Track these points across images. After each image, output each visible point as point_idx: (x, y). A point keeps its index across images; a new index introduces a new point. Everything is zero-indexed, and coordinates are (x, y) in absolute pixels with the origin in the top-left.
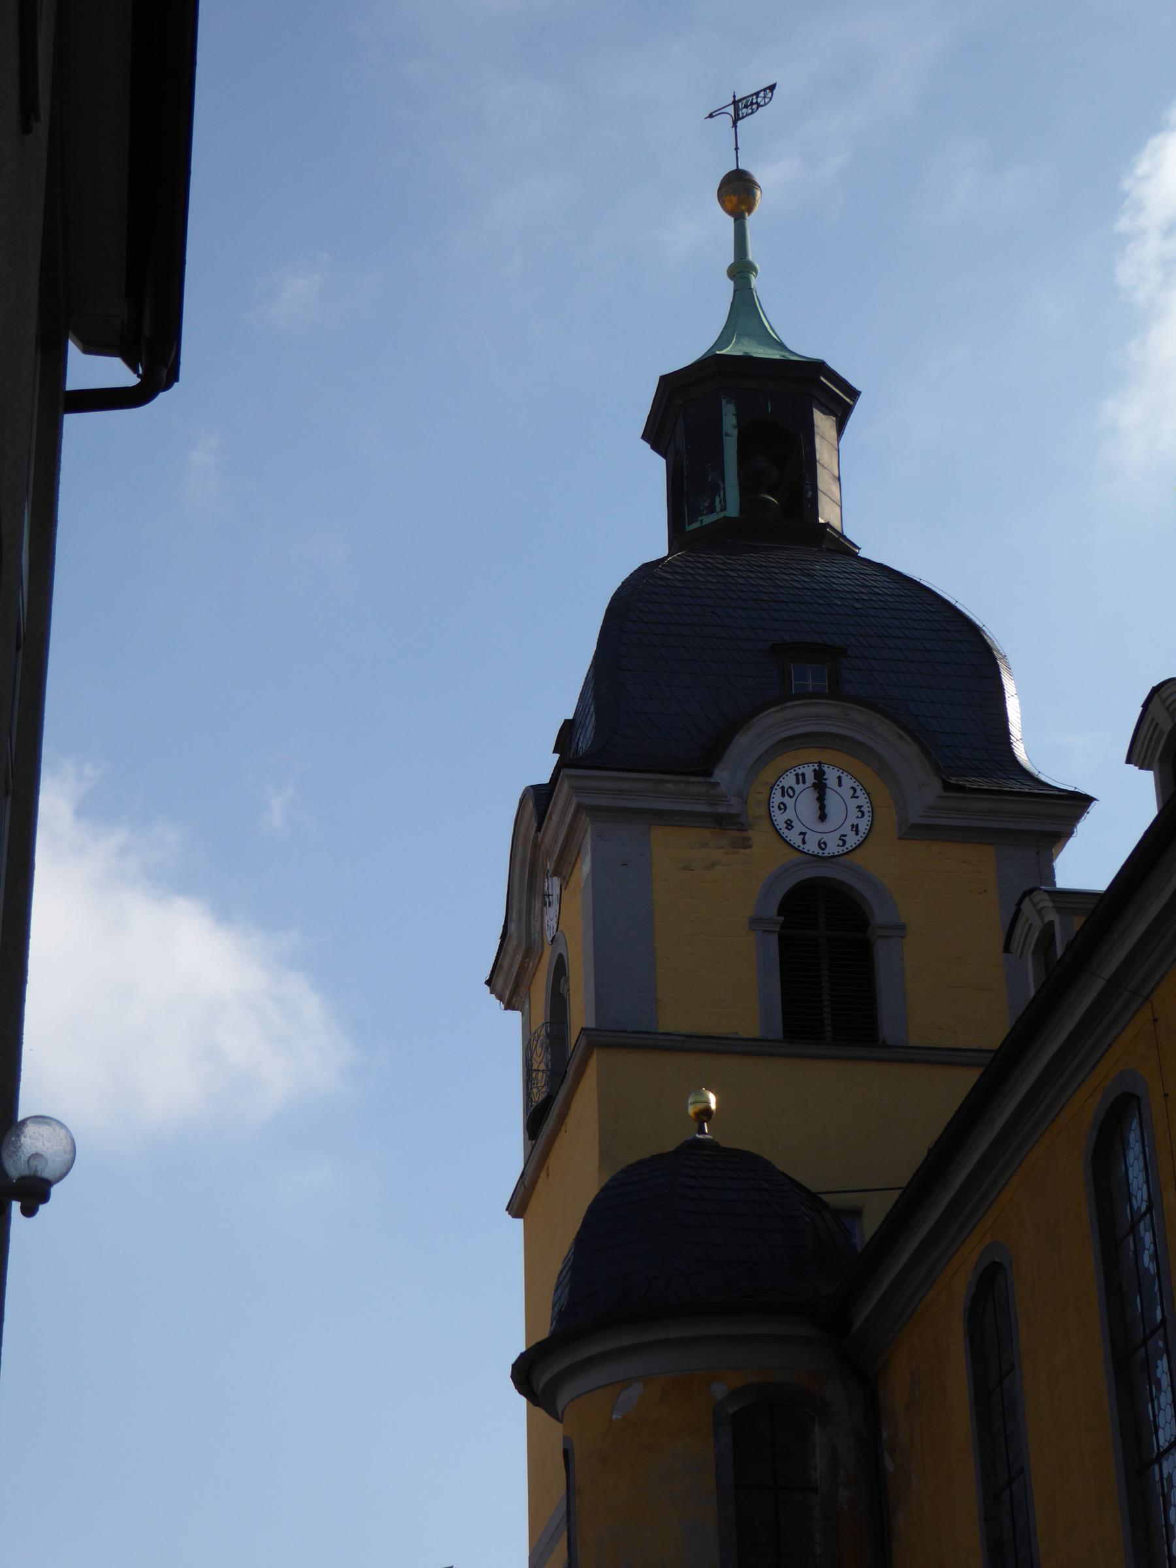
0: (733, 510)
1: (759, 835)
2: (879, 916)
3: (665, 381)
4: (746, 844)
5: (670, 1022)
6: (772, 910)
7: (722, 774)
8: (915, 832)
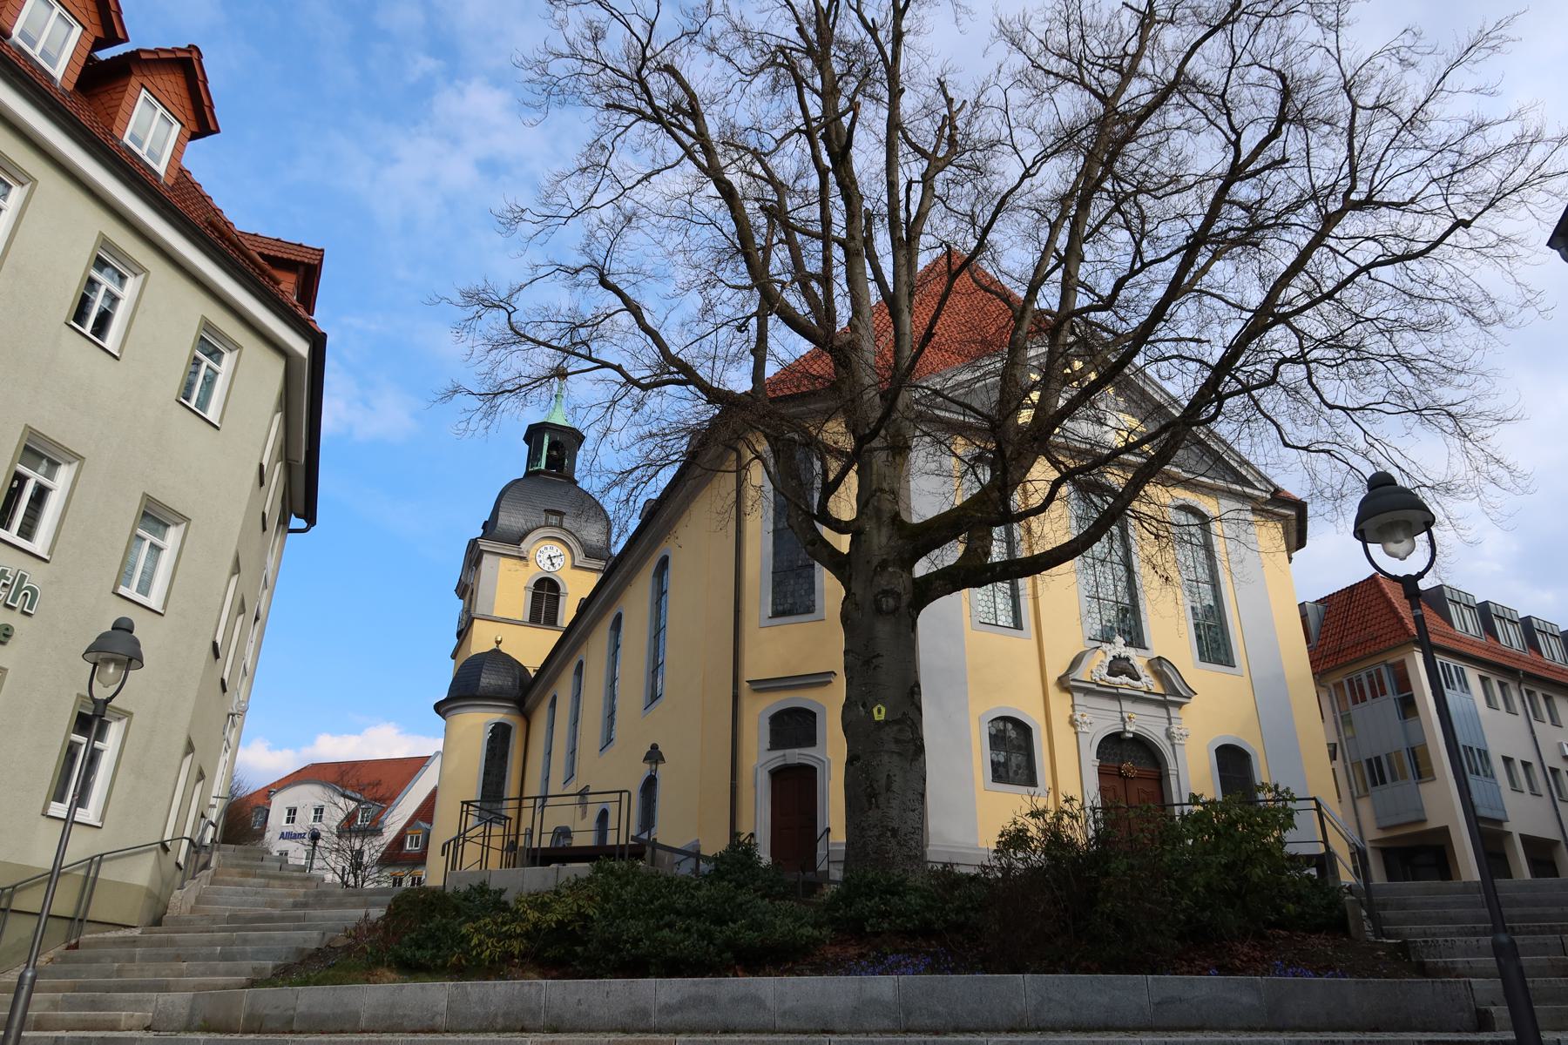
0: (543, 467)
1: (532, 564)
2: (562, 590)
3: (530, 426)
4: (527, 565)
5: (497, 614)
6: (532, 585)
7: (522, 545)
8: (575, 567)
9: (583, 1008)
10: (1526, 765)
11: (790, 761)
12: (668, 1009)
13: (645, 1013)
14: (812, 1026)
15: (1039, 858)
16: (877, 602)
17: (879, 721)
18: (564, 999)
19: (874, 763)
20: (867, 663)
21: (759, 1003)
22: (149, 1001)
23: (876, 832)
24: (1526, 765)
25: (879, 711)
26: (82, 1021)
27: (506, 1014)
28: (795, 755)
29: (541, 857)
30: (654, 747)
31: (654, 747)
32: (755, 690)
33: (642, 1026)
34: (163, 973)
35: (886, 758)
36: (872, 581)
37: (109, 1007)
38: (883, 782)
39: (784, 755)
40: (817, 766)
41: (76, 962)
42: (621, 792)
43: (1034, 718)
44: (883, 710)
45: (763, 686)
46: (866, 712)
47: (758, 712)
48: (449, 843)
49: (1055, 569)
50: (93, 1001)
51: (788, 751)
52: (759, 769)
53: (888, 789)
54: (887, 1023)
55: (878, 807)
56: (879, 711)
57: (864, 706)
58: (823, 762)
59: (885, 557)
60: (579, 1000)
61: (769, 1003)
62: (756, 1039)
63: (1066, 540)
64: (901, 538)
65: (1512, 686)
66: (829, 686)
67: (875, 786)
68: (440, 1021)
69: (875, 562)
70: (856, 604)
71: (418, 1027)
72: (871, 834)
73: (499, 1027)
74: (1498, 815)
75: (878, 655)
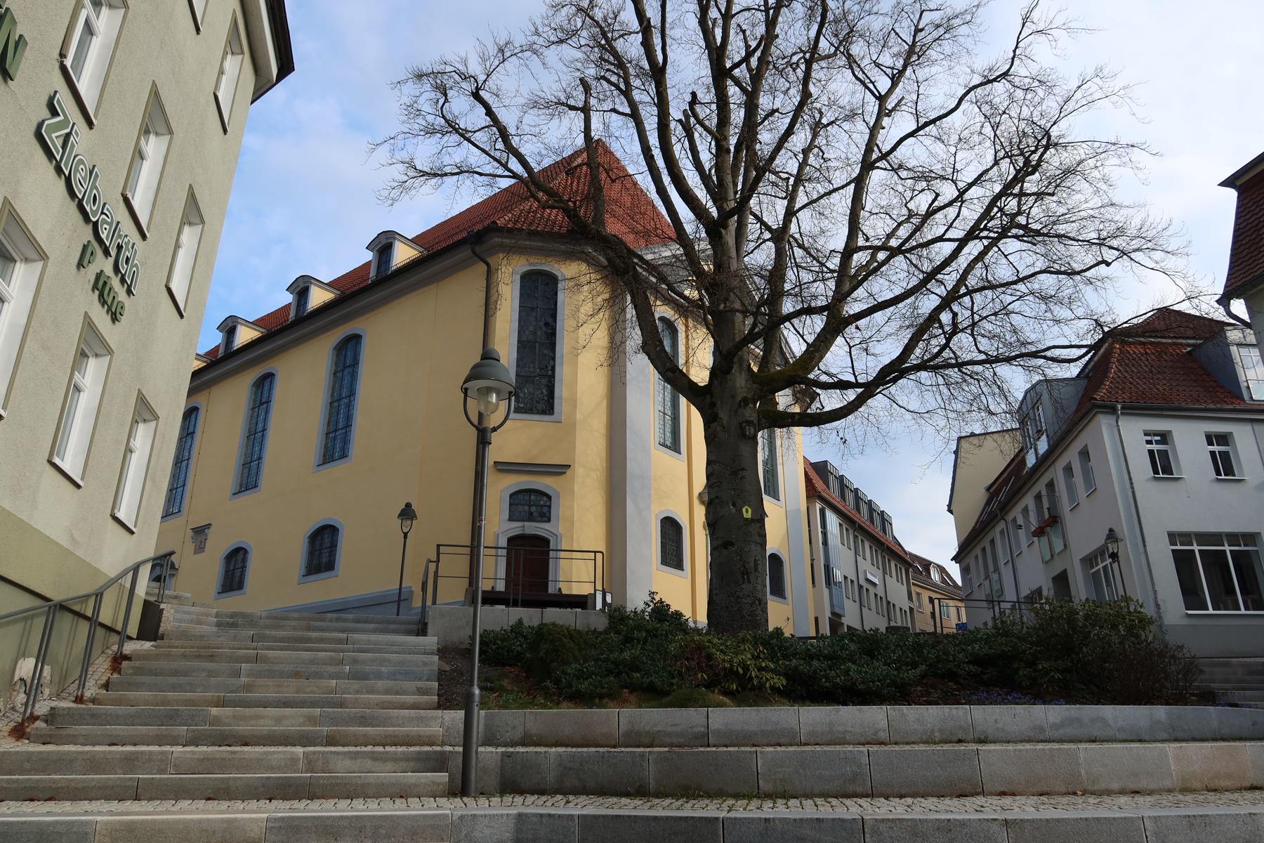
9: (1000, 725)
10: (852, 581)
11: (527, 532)
12: (1055, 726)
13: (1042, 729)
14: (1133, 738)
15: (601, 623)
16: (742, 429)
17: (747, 519)
18: (985, 719)
19: (746, 549)
20: (735, 473)
21: (1104, 721)
22: (435, 719)
23: (749, 600)
24: (852, 581)
25: (747, 511)
26: (390, 736)
27: (941, 731)
28: (532, 528)
29: (522, 601)
30: (408, 505)
31: (408, 505)
32: (499, 470)
33: (1041, 737)
34: (307, 690)
35: (753, 546)
36: (736, 411)
37: (383, 722)
38: (752, 564)
39: (524, 526)
40: (551, 539)
41: (156, 675)
42: (595, 552)
43: (684, 521)
44: (750, 511)
45: (504, 467)
46: (736, 510)
47: (498, 490)
48: (136, 569)
49: (827, 425)
50: (361, 717)
51: (527, 524)
52: (500, 535)
53: (756, 570)
54: (1165, 736)
55: (749, 582)
56: (747, 511)
57: (734, 505)
58: (556, 535)
59: (745, 395)
60: (996, 720)
61: (1111, 722)
62: (1061, 747)
63: (838, 406)
64: (754, 383)
65: (851, 531)
66: (563, 476)
67: (747, 566)
68: (883, 735)
69: (739, 398)
70: (723, 427)
71: (862, 740)
72: (746, 601)
73: (937, 739)
74: (841, 613)
75: (743, 469)
